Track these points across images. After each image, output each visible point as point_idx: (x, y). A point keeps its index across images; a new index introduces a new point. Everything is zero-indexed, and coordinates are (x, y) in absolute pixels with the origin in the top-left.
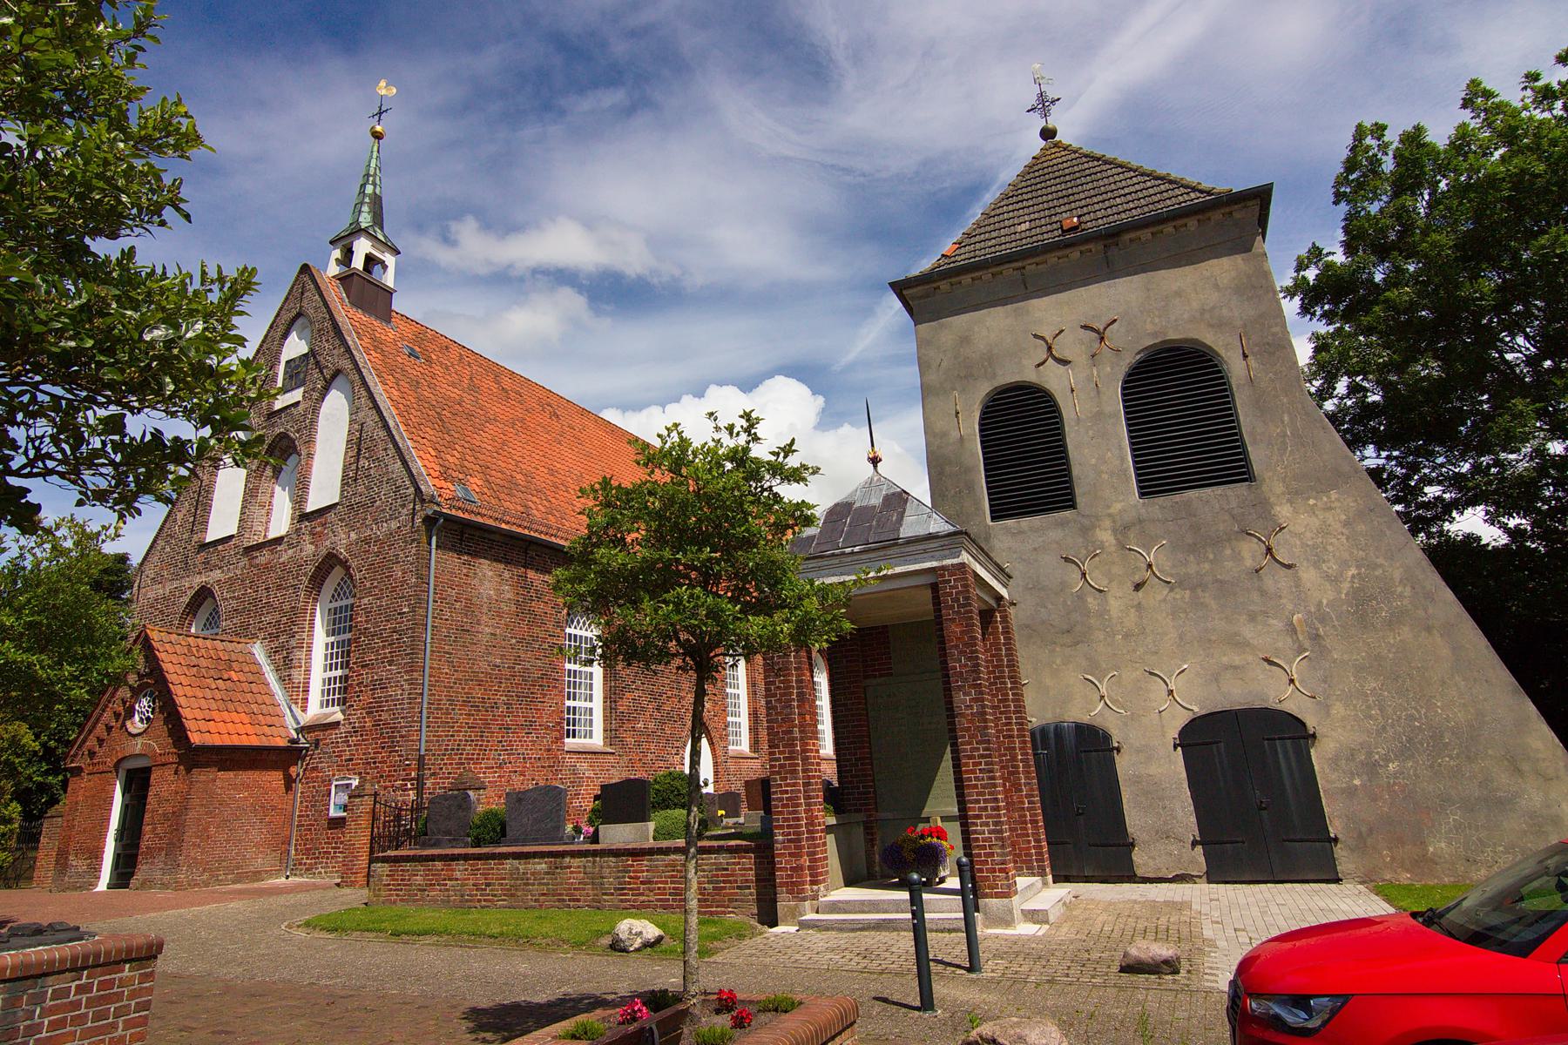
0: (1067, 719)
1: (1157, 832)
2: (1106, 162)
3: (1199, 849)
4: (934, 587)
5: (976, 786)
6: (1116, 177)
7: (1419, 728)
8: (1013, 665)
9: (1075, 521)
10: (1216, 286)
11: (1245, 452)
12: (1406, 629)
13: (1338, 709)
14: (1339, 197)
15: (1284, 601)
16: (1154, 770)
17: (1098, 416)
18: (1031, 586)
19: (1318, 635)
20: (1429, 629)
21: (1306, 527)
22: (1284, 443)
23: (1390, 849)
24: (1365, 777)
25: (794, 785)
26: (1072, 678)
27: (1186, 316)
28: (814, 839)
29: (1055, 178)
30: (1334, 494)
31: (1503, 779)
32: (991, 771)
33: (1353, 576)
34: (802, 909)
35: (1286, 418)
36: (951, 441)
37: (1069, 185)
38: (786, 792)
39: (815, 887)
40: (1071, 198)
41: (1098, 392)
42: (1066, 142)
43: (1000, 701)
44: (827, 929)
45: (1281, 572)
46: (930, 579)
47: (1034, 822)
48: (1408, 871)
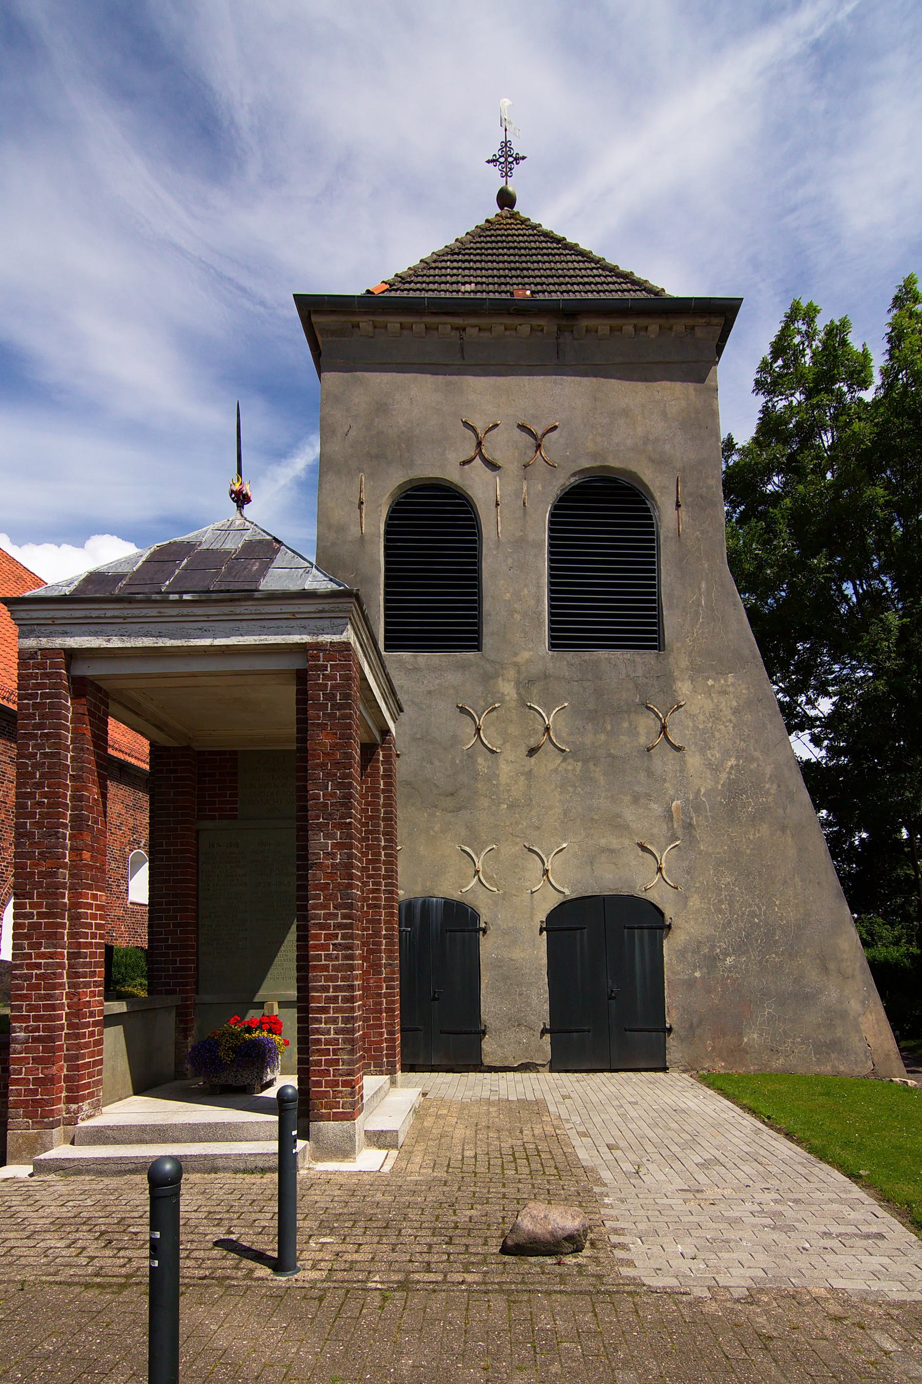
0: (437, 894)
1: (510, 1020)
3: (547, 1037)
4: (301, 677)
5: (325, 968)
6: (576, 265)
7: (758, 924)
8: (390, 819)
10: (664, 414)
12: (765, 826)
13: (695, 902)
15: (667, 785)
16: (517, 954)
17: (520, 543)
18: (418, 736)
19: (690, 824)
20: (783, 829)
21: (700, 708)
22: (697, 613)
23: (713, 1039)
24: (705, 970)
25: (51, 956)
26: (449, 847)
27: (629, 442)
28: (78, 1036)
29: (499, 270)
30: (731, 678)
31: (813, 976)
33: (732, 767)
34: (46, 1139)
36: (350, 538)
37: (523, 258)
38: (38, 966)
39: (74, 1107)
40: (525, 273)
41: (525, 513)
42: (524, 215)
43: (369, 862)
44: (79, 1172)
45: (671, 754)
46: (294, 663)
47: (390, 1010)
48: (723, 1060)
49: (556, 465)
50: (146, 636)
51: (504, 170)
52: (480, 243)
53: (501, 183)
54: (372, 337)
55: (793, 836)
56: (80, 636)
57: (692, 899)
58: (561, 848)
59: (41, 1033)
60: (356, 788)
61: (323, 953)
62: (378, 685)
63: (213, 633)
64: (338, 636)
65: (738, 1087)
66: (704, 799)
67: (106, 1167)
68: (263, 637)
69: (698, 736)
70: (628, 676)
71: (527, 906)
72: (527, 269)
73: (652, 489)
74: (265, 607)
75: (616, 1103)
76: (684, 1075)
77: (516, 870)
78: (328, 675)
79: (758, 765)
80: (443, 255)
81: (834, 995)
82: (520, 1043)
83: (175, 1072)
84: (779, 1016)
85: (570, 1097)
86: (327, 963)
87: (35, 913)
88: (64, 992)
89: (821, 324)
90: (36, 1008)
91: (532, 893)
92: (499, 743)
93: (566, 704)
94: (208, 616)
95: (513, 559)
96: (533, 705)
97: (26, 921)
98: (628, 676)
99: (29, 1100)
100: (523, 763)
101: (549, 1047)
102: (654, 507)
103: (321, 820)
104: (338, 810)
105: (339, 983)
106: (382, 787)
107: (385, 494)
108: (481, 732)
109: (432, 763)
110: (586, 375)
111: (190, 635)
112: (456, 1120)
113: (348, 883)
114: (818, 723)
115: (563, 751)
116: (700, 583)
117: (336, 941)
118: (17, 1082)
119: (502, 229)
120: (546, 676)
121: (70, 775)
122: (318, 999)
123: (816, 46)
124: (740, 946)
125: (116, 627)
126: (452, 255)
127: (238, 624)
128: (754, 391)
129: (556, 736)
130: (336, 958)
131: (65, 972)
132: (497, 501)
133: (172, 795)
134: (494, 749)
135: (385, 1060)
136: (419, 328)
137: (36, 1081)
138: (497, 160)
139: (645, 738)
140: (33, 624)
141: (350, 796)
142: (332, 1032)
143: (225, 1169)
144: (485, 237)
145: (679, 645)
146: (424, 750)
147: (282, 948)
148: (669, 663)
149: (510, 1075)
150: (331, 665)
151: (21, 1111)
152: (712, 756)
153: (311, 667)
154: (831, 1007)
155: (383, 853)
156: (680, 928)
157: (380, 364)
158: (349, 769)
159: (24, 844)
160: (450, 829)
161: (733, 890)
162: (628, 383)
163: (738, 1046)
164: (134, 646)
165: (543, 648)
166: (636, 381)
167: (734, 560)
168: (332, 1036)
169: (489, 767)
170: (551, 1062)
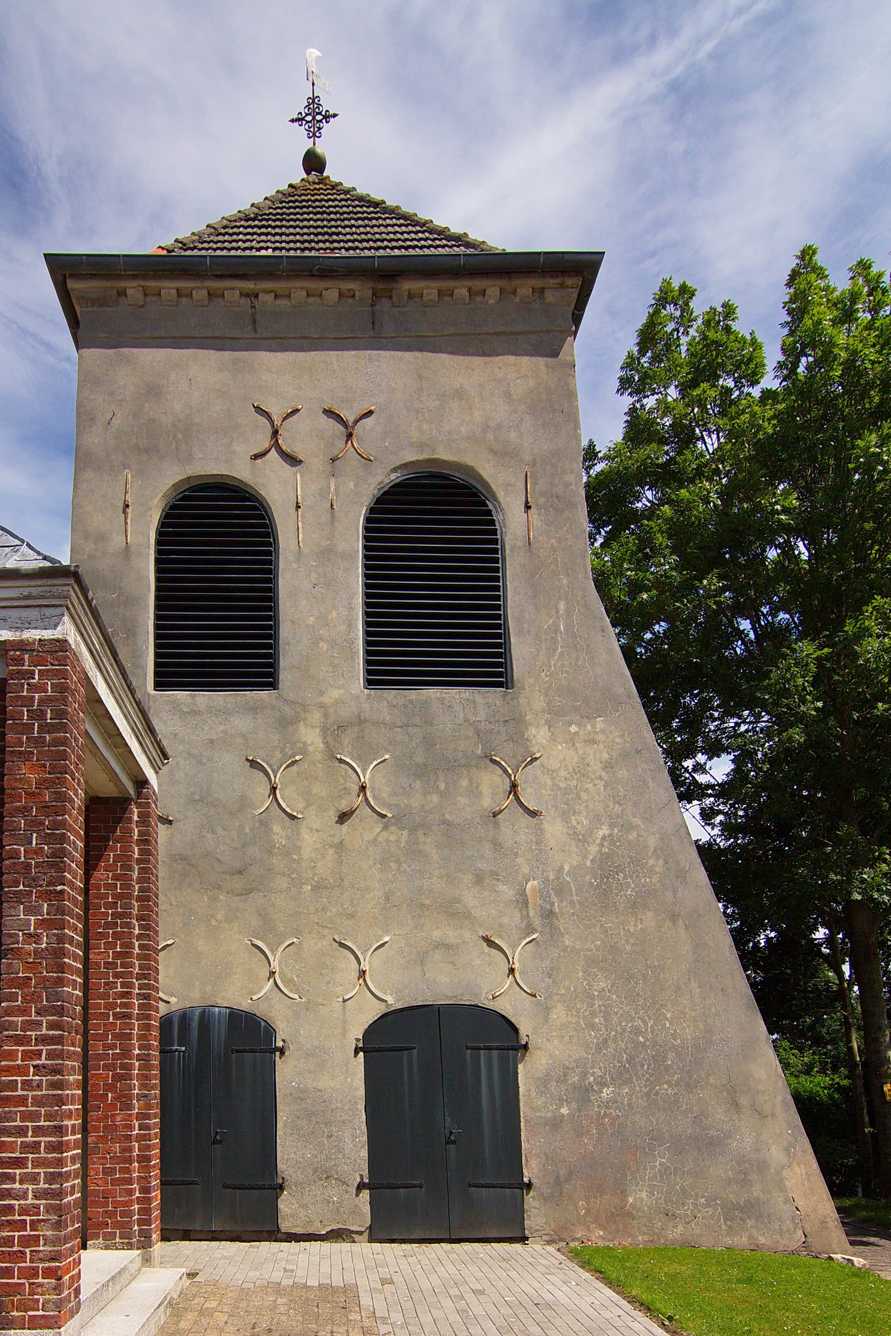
1: (315, 1171)
2: (386, 210)
3: (366, 1194)
5: (23, 1100)
8: (147, 898)
9: (273, 708)
10: (508, 395)
11: (506, 645)
12: (650, 914)
13: (559, 1014)
14: (625, 384)
15: (520, 860)
16: (325, 1082)
17: (327, 554)
18: (197, 797)
19: (551, 912)
20: (674, 918)
21: (561, 762)
22: (554, 641)
23: (587, 1199)
24: (574, 1105)
30: (600, 723)
31: (719, 1114)
32: (57, 1071)
33: (604, 838)
35: (562, 606)
36: (111, 550)
41: (333, 517)
42: (334, 179)
43: (117, 955)
47: (144, 1159)
48: (601, 1227)
49: (372, 458)
51: (312, 129)
52: (281, 208)
53: (309, 144)
54: (143, 306)
55: (687, 928)
57: (556, 1011)
58: (382, 942)
60: (74, 843)
61: (19, 1078)
62: (125, 716)
64: (50, 632)
65: (624, 1268)
66: (568, 879)
69: (559, 797)
70: (466, 720)
71: (338, 1019)
72: (338, 234)
73: (493, 487)
75: (454, 1292)
76: (549, 1248)
77: (323, 971)
78: (35, 685)
79: (638, 835)
80: (235, 221)
81: (748, 1140)
82: (329, 1202)
84: (675, 1168)
85: (391, 1282)
89: (699, 306)
91: (344, 1001)
92: (301, 806)
93: (387, 757)
95: (319, 574)
96: (343, 758)
98: (466, 720)
100: (332, 832)
101: (368, 1208)
102: (496, 508)
103: (21, 887)
104: (45, 874)
105: (42, 1123)
106: (136, 856)
107: (157, 495)
108: (278, 792)
109: (213, 832)
110: (409, 349)
112: (226, 1317)
113: (58, 977)
114: (710, 791)
115: (383, 816)
116: (557, 603)
119: (308, 194)
120: (360, 721)
123: (675, 87)
124: (620, 1073)
126: (247, 221)
128: (618, 391)
129: (374, 798)
132: (297, 503)
134: (295, 814)
135: (136, 1227)
136: (200, 294)
138: (303, 119)
139: (489, 800)
141: (63, 853)
142: (30, 1196)
144: (288, 203)
145: (532, 681)
146: (203, 814)
148: (519, 703)
149: (315, 1245)
150: (40, 671)
152: (578, 823)
153: (13, 675)
154: (744, 1156)
155: (137, 944)
156: (540, 1049)
157: (152, 338)
158: (63, 815)
160: (237, 918)
161: (609, 998)
162: (462, 358)
163: (622, 1208)
165: (356, 684)
166: (473, 355)
167: (602, 582)
168: (30, 1201)
169: (288, 837)
170: (370, 1228)
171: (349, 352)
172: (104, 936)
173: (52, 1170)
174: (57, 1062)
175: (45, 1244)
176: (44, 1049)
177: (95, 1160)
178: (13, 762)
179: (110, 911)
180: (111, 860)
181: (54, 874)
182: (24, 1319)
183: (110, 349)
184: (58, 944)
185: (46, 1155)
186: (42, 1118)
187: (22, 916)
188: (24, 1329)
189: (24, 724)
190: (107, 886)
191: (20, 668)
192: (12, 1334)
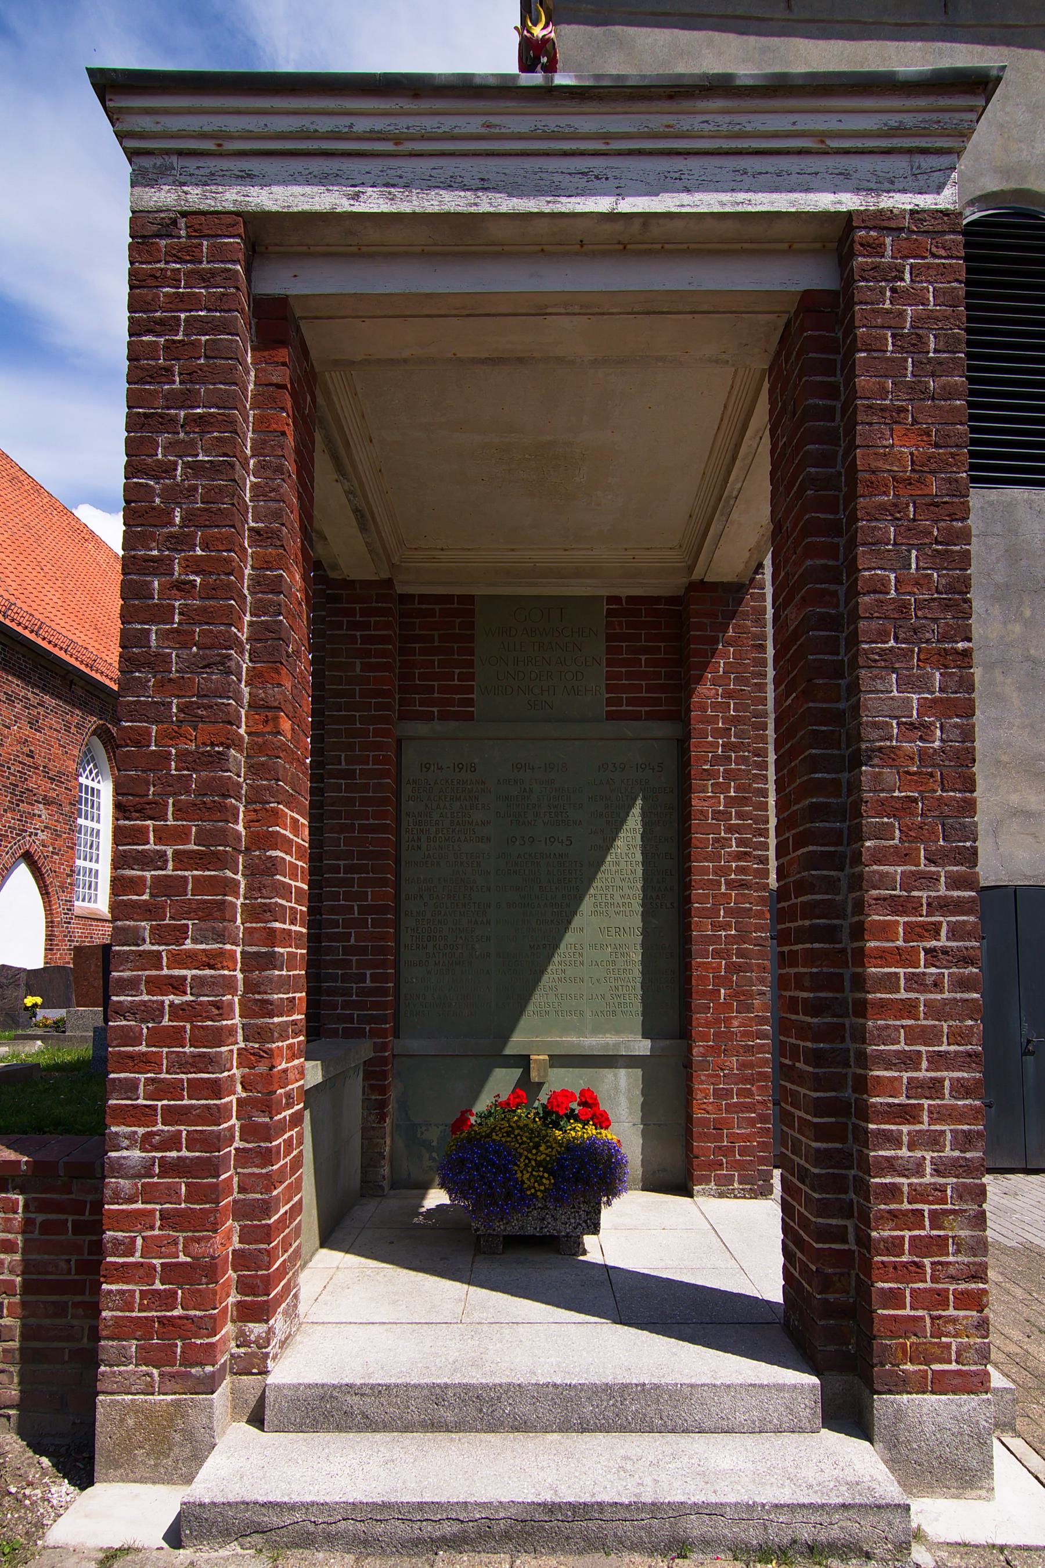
5: (908, 1009)
25: (211, 960)
38: (177, 985)
39: (256, 1329)
43: (730, 802)
44: (306, 1540)
50: (449, 187)
56: (285, 183)
59: (184, 1153)
61: (901, 971)
63: (617, 183)
67: (380, 1528)
68: (741, 196)
74: (752, 117)
78: (905, 291)
83: (362, 1181)
86: (912, 995)
87: (170, 852)
88: (235, 1048)
90: (171, 1090)
94: (607, 137)
97: (148, 874)
99: (151, 1319)
103: (892, 643)
104: (935, 620)
111: (558, 188)
117: (934, 943)
118: (123, 1273)
121: (251, 529)
122: (890, 1087)
125: (374, 165)
127: (679, 163)
130: (935, 985)
131: (236, 999)
133: (358, 669)
137: (171, 1272)
140: (168, 152)
142: (928, 1170)
143: (707, 1544)
147: (556, 959)
150: (912, 266)
151: (133, 1345)
159: (143, 684)
164: (418, 210)
168: (928, 1179)
171: (912, 44)
172: (711, 774)
173: (965, 1127)
174: (968, 944)
175: (957, 1252)
176: (944, 921)
177: (703, 1078)
178: (870, 424)
179: (720, 741)
180: (721, 669)
181: (951, 622)
182: (925, 1377)
183: (598, 25)
184: (963, 742)
185: (953, 1102)
186: (945, 1039)
187: (895, 693)
188: (924, 1393)
189: (888, 358)
190: (715, 706)
191: (878, 260)
192: (905, 1402)
